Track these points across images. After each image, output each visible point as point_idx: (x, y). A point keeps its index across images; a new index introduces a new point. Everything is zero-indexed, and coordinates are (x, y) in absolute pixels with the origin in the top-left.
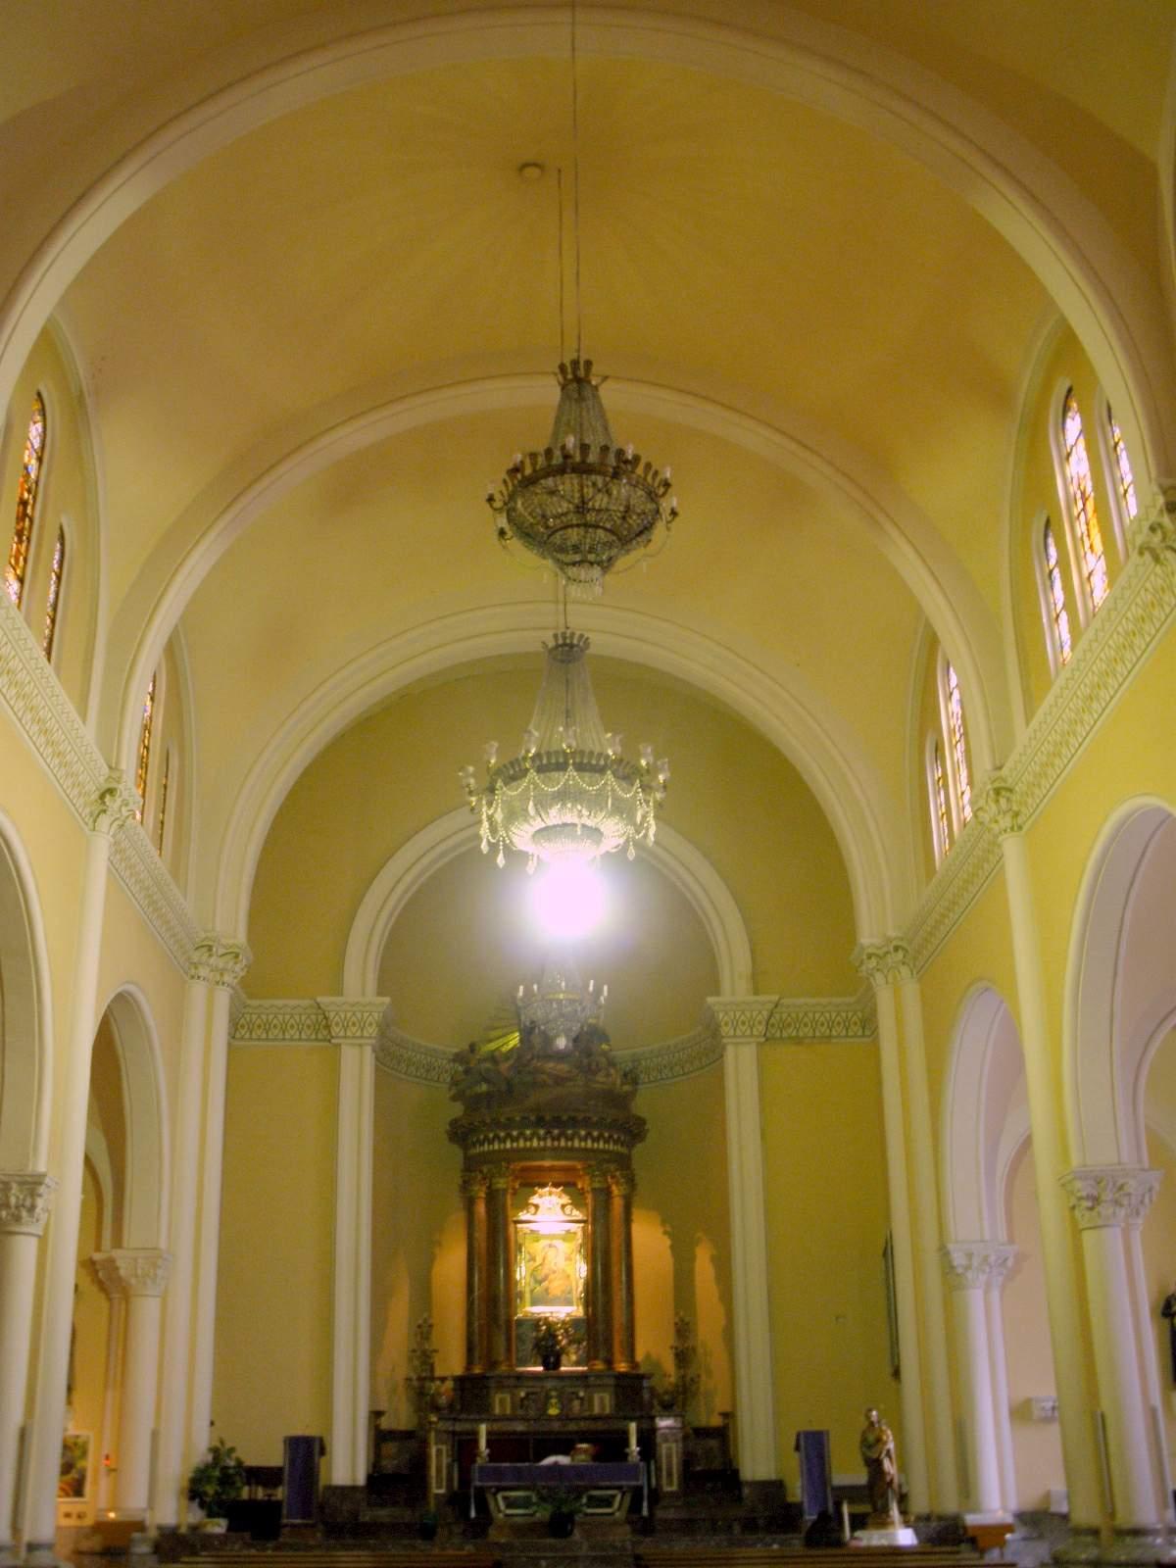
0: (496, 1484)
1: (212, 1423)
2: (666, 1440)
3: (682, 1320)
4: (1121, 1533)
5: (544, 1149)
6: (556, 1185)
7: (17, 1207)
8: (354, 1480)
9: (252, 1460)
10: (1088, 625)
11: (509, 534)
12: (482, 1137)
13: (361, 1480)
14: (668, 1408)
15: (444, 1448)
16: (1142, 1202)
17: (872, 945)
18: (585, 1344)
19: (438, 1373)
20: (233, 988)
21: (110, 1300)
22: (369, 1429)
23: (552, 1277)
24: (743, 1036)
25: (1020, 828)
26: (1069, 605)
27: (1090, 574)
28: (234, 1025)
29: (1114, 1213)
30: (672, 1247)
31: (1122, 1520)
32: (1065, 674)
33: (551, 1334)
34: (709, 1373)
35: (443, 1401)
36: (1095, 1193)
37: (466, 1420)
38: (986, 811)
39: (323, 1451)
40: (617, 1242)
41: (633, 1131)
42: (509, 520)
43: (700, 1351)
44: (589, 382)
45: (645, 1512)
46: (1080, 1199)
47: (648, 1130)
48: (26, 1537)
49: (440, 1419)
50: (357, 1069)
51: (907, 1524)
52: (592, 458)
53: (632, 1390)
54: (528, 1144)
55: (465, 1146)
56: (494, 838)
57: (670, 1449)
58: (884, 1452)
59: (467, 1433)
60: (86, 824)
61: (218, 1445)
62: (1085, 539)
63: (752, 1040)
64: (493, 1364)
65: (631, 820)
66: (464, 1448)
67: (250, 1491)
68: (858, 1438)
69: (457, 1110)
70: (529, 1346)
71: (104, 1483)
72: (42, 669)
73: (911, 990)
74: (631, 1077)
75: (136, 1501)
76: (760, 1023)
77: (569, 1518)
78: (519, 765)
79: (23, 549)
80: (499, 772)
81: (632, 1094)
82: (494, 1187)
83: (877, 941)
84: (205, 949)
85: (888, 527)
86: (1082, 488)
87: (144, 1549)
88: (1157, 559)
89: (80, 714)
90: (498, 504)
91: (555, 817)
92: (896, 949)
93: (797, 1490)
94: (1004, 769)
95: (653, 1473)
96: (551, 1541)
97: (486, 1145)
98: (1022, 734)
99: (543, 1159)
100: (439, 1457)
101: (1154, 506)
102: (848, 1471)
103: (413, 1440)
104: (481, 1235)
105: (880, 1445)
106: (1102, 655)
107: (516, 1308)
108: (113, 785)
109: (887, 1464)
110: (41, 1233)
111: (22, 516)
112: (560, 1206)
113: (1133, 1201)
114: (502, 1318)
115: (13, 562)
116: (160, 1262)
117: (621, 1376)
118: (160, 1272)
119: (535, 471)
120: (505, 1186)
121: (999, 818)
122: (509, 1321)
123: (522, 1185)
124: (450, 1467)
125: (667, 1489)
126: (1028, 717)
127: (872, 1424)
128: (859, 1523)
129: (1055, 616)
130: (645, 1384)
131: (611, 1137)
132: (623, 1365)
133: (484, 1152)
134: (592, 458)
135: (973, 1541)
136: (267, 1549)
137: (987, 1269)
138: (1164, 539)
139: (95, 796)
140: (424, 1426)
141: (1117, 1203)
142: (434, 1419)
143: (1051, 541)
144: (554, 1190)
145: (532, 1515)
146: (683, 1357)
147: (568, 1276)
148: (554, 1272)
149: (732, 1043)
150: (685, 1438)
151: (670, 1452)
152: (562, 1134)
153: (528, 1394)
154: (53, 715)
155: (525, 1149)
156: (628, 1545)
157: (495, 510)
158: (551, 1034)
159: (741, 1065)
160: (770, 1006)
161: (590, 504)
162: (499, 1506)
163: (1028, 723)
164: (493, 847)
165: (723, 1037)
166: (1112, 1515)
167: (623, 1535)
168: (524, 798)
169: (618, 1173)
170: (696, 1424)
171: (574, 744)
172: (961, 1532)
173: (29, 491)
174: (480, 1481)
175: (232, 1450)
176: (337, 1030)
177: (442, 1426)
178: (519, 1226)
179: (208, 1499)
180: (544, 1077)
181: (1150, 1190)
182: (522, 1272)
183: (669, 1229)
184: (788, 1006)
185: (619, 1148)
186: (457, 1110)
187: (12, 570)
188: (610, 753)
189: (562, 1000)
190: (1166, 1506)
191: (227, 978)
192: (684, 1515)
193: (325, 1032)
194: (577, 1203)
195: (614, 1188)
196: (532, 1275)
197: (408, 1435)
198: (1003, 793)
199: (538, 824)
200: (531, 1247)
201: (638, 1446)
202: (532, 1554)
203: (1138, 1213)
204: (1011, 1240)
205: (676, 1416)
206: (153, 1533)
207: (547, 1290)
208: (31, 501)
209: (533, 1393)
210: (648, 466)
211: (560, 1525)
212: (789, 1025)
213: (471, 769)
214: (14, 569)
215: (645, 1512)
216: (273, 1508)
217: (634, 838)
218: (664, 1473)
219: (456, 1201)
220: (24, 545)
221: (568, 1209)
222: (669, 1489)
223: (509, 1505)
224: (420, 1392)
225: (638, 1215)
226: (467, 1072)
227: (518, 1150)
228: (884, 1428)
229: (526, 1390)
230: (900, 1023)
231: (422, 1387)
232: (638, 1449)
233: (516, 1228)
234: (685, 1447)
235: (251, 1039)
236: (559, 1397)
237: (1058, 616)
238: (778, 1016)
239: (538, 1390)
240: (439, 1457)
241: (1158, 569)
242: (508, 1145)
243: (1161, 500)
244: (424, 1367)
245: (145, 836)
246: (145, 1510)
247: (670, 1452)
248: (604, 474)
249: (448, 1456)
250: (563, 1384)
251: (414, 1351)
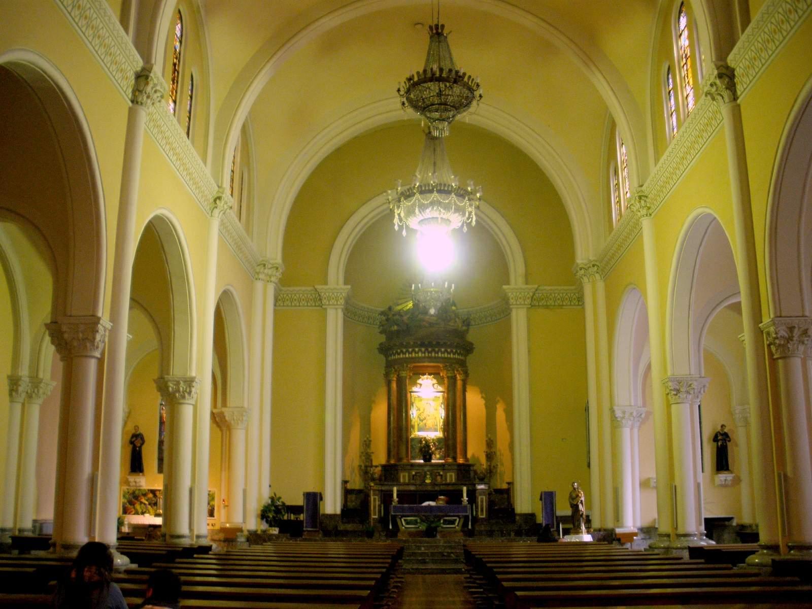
0: (401, 514)
1: (270, 486)
2: (480, 495)
3: (490, 439)
4: (679, 536)
5: (424, 357)
6: (430, 374)
7: (183, 392)
8: (335, 510)
9: (289, 503)
10: (685, 120)
11: (407, 104)
12: (394, 352)
13: (338, 511)
14: (482, 480)
15: (377, 497)
16: (700, 392)
17: (582, 263)
18: (443, 450)
19: (374, 463)
20: (275, 283)
21: (221, 430)
22: (342, 488)
23: (428, 418)
24: (520, 304)
25: (650, 215)
26: (677, 110)
27: (687, 96)
28: (276, 300)
29: (686, 397)
31: (681, 531)
32: (674, 141)
33: (427, 446)
34: (502, 464)
35: (376, 476)
36: (678, 387)
37: (386, 485)
38: (634, 206)
39: (321, 499)
40: (459, 402)
41: (468, 349)
42: (407, 99)
43: (498, 453)
44: (443, 35)
45: (470, 527)
46: (671, 390)
48: (196, 533)
49: (375, 484)
50: (335, 320)
51: (588, 532)
52: (444, 75)
53: (466, 472)
55: (387, 356)
56: (401, 223)
57: (482, 499)
58: (580, 501)
59: (387, 491)
60: (208, 213)
61: (273, 495)
62: (686, 78)
63: (525, 306)
64: (400, 459)
65: (464, 215)
66: (386, 498)
67: (288, 516)
68: (568, 495)
69: (383, 338)
70: (417, 451)
71: (223, 511)
72: (185, 142)
73: (601, 285)
74: (467, 323)
75: (237, 519)
76: (528, 298)
77: (435, 529)
78: (412, 190)
79: (175, 87)
80: (402, 194)
81: (467, 331)
82: (400, 376)
83: (585, 261)
84: (262, 266)
85: (594, 68)
86: (686, 52)
87: (243, 539)
88: (713, 99)
89: (203, 160)
90: (402, 93)
91: (428, 214)
92: (594, 266)
93: (540, 519)
94: (644, 187)
95: (474, 510)
96: (427, 539)
97: (396, 356)
98: (653, 170)
99: (424, 362)
100: (375, 501)
101: (713, 74)
102: (563, 509)
103: (363, 495)
105: (578, 498)
106: (697, 128)
107: (411, 432)
108: (220, 195)
109: (580, 506)
110: (194, 403)
111: (175, 70)
112: (432, 384)
113: (696, 391)
114: (404, 436)
115: (171, 93)
116: (244, 414)
117: (460, 465)
118: (244, 418)
119: (419, 79)
120: (406, 375)
121: (641, 210)
122: (407, 438)
123: (414, 374)
124: (380, 506)
125: (481, 517)
126: (657, 160)
127: (574, 489)
128: (566, 532)
129: (670, 113)
130: (472, 468)
131: (456, 351)
132: (461, 460)
133: (395, 359)
134: (444, 75)
135: (619, 540)
136: (297, 541)
137: (632, 418)
138: (716, 90)
139: (212, 200)
140: (368, 488)
141: (688, 392)
142: (372, 484)
143: (670, 76)
144: (429, 377)
145: (418, 528)
146: (490, 456)
147: (436, 418)
148: (429, 416)
149: (516, 308)
150: (490, 494)
151: (482, 500)
153: (416, 473)
154: (176, 140)
156: (462, 541)
157: (401, 95)
158: (427, 307)
159: (519, 319)
160: (534, 290)
161: (444, 93)
162: (403, 524)
163: (656, 165)
164: (401, 227)
165: (510, 305)
166: (676, 528)
167: (460, 538)
168: (414, 205)
169: (459, 369)
170: (495, 488)
171: (436, 181)
172: (614, 536)
173: (176, 58)
174: (394, 512)
175: (280, 498)
176: (325, 301)
177: (376, 487)
178: (412, 394)
179: (269, 520)
180: (424, 323)
181: (704, 386)
182: (414, 413)
183: (484, 395)
184: (542, 290)
185: (460, 357)
186: (383, 338)
187: (170, 97)
188: (453, 185)
189: (432, 292)
190: (700, 525)
191: (273, 279)
192: (488, 528)
193: (319, 302)
194: (440, 382)
195: (458, 376)
196: (418, 417)
197: (359, 491)
198: (643, 198)
199: (420, 217)
200: (417, 404)
201: (467, 497)
202: (418, 545)
203: (698, 397)
204: (644, 405)
205: (485, 484)
206: (246, 533)
207: (425, 424)
208: (177, 63)
209: (418, 473)
210: (470, 77)
211: (430, 532)
212: (543, 299)
213: (389, 192)
214: (172, 97)
215: (470, 527)
216: (300, 523)
217: (466, 222)
218: (479, 509)
219: (382, 381)
220: (175, 85)
221: (436, 385)
222: (482, 517)
223: (408, 523)
224: (366, 471)
226: (387, 320)
227: (412, 358)
228: (580, 491)
229: (416, 471)
230: (595, 303)
231: (367, 469)
232: (467, 499)
233: (411, 395)
234: (489, 498)
235: (284, 306)
236: (431, 474)
237: (672, 113)
238: (537, 295)
239: (421, 471)
240: (375, 501)
241: (714, 102)
242: (407, 356)
243: (716, 72)
244: (367, 460)
245: (233, 214)
246: (242, 523)
247: (482, 500)
248: (449, 82)
249: (378, 501)
250: (433, 468)
251: (362, 453)
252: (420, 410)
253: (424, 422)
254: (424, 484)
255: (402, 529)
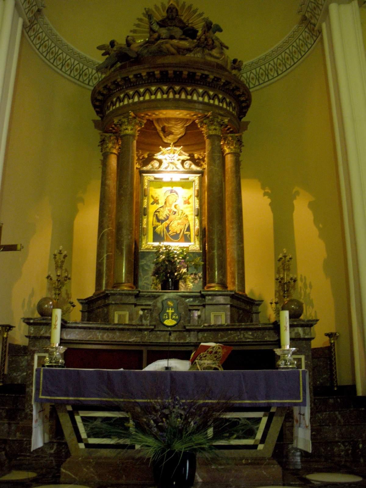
5: (167, 100)
23: (172, 217)
30: (271, 204)
34: (311, 304)
47: (247, 123)
54: (153, 97)
104: (112, 182)
112: (180, 161)
131: (224, 99)
147: (187, 216)
152: (183, 89)
155: (150, 101)
207: (167, 228)
221: (187, 164)
225: (244, 183)
252: (158, 203)
253: (165, 224)
254: (162, 328)
255: (78, 449)
